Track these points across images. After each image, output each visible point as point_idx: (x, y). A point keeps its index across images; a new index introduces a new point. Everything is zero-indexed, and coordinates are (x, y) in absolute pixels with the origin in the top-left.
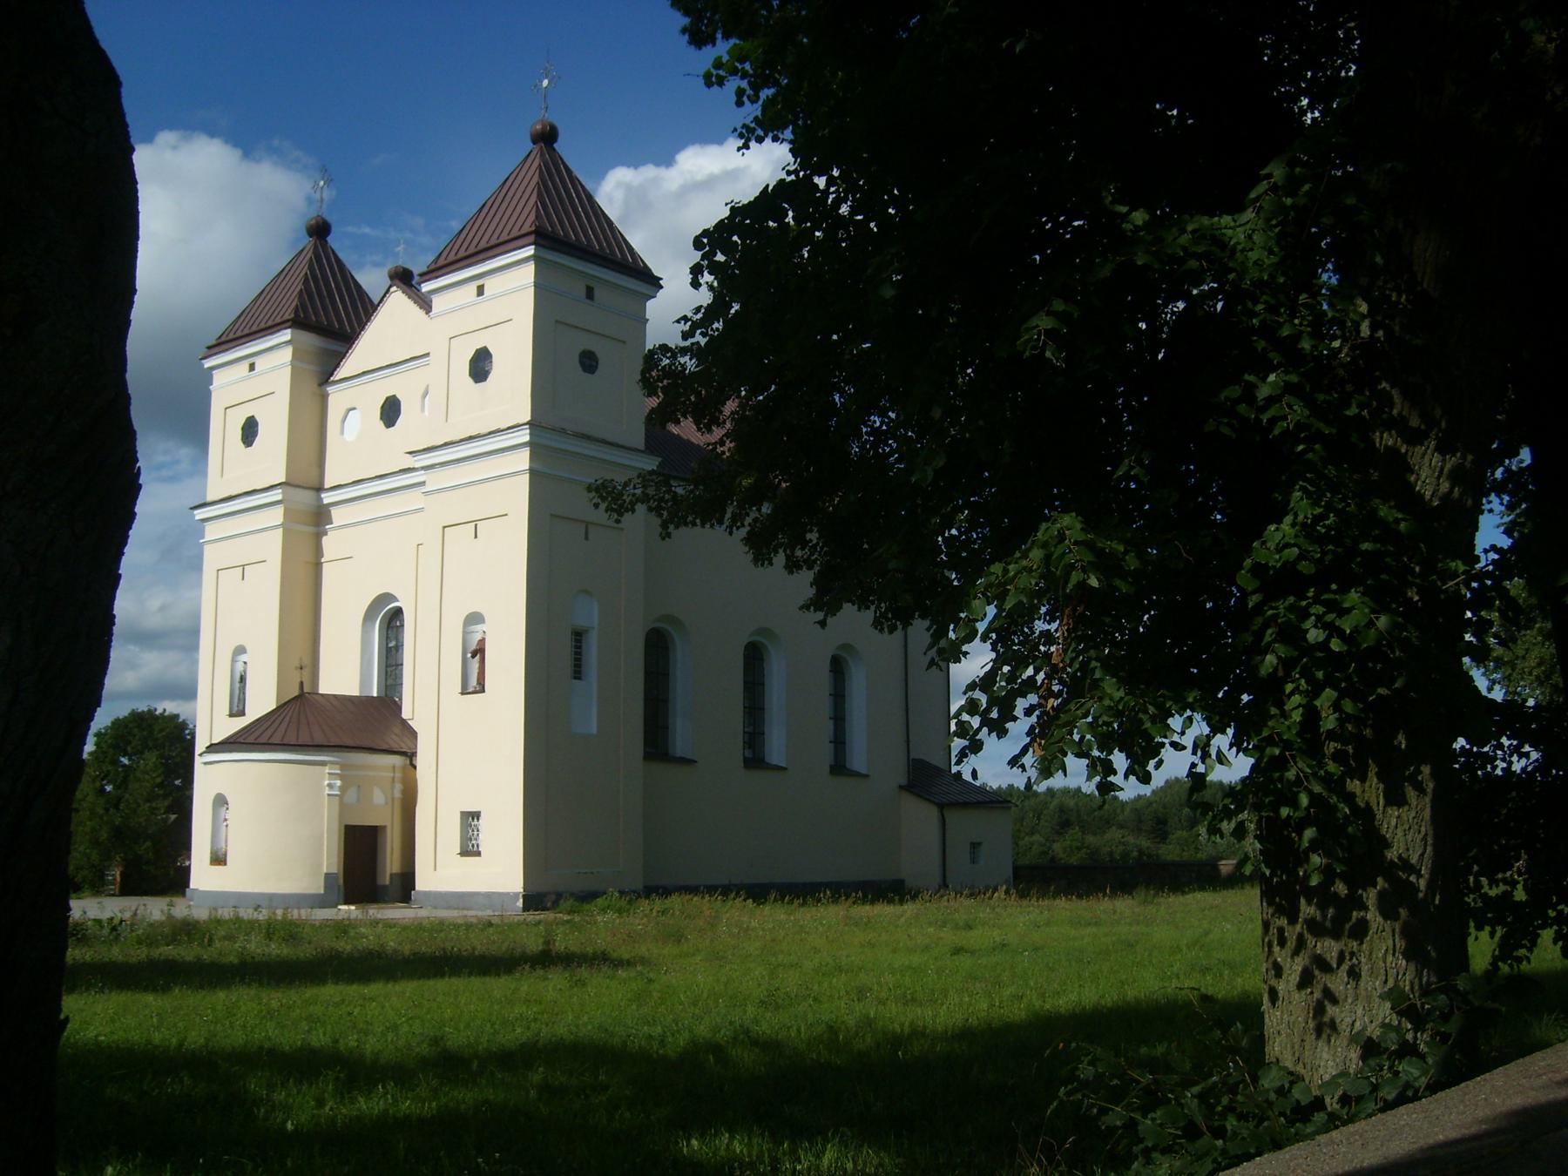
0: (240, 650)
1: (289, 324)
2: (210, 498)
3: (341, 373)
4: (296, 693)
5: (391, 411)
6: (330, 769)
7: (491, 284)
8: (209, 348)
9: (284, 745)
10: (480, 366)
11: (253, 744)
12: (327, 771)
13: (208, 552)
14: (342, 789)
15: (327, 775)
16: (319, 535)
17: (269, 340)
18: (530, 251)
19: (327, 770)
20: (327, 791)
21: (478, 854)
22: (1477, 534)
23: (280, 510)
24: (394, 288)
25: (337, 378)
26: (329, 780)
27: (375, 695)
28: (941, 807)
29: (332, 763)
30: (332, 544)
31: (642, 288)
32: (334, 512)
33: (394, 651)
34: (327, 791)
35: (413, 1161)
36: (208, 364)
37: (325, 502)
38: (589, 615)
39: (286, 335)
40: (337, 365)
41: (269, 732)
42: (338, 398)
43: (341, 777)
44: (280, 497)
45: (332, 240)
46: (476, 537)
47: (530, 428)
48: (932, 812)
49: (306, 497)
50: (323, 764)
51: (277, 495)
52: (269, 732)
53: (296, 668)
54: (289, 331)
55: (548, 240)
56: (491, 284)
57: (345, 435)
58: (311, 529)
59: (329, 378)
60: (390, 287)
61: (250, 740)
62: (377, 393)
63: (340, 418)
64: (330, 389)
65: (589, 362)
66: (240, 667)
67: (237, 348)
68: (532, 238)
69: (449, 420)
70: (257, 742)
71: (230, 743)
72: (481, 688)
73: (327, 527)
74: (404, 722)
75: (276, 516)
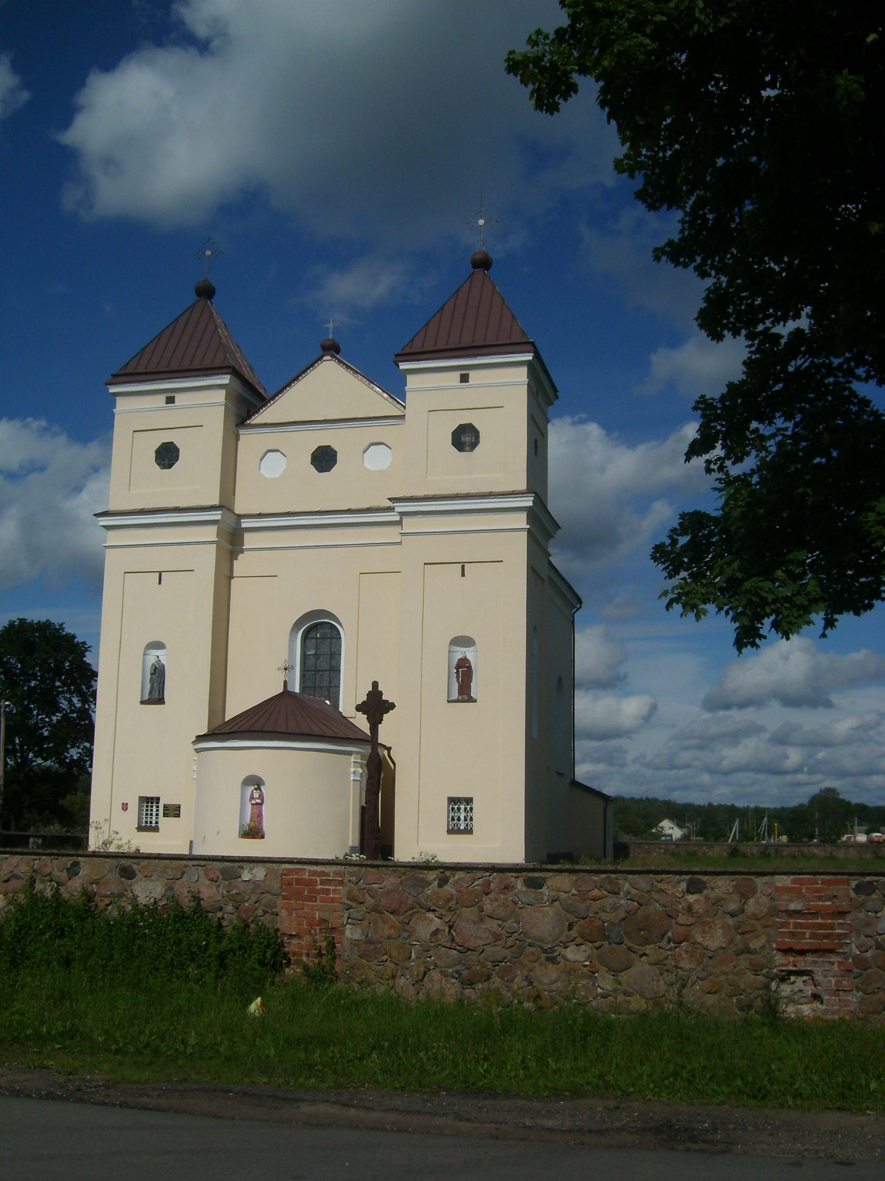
1: (231, 370)
2: (113, 507)
3: (257, 419)
4: (281, 690)
6: (354, 758)
7: (475, 376)
8: (114, 376)
9: (289, 733)
11: (229, 733)
12: (353, 760)
15: (353, 764)
17: (203, 380)
19: (352, 759)
22: (472, 683)
23: (214, 529)
24: (328, 358)
26: (354, 767)
29: (356, 753)
30: (241, 565)
32: (247, 537)
35: (479, 1105)
36: (113, 390)
37: (244, 525)
40: (257, 412)
44: (219, 517)
47: (534, 497)
50: (350, 753)
51: (216, 516)
52: (237, 727)
54: (229, 376)
56: (473, 375)
58: (229, 547)
59: (246, 421)
63: (261, 456)
66: (151, 660)
67: (157, 382)
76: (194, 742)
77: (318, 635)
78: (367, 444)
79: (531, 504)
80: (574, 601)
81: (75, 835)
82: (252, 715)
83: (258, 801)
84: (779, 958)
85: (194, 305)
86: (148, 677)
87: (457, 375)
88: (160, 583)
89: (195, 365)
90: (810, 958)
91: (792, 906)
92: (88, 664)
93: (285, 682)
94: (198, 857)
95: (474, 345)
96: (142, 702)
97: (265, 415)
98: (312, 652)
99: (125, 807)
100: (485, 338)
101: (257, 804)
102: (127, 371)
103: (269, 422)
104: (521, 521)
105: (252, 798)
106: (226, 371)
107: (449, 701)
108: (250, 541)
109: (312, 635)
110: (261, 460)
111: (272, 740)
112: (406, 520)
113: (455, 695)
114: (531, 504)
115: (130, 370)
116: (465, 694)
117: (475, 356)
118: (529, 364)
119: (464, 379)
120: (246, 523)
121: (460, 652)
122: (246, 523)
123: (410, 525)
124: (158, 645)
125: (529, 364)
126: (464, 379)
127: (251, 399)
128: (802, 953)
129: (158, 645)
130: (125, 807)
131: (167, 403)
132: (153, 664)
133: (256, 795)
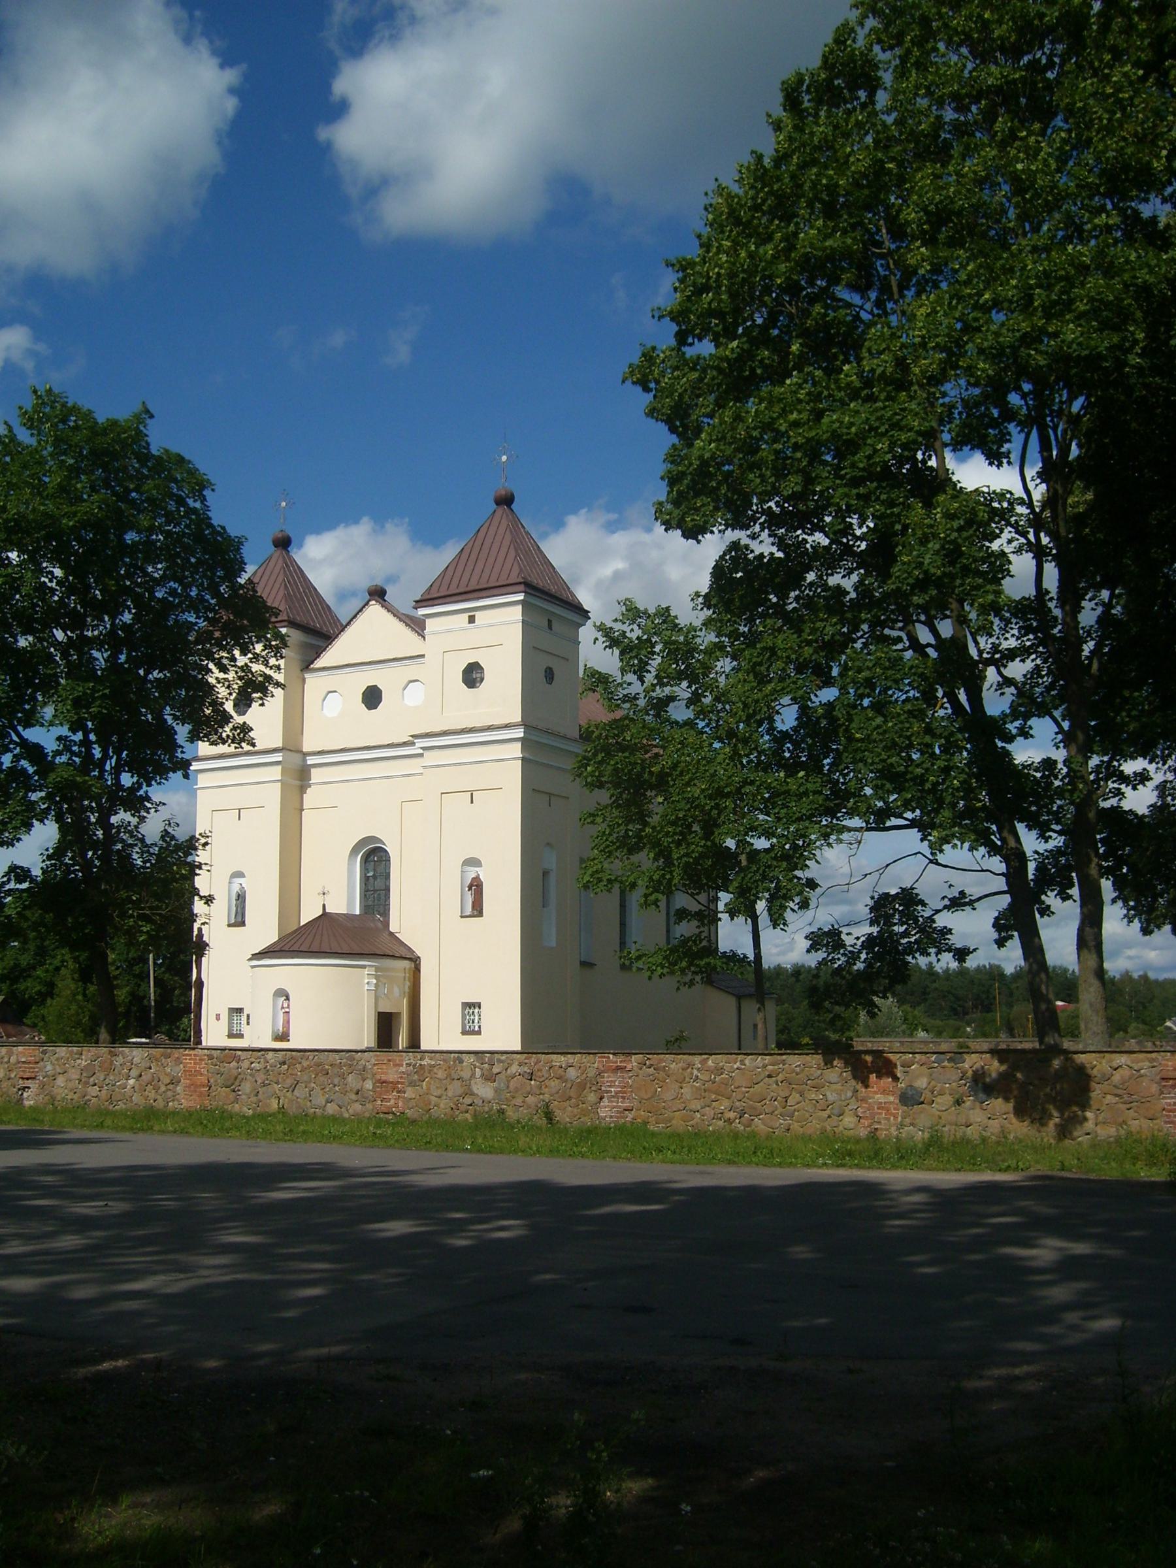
1: (286, 624)
3: (319, 664)
4: (320, 913)
5: (372, 697)
10: (472, 675)
14: (376, 985)
16: (303, 789)
18: (521, 597)
19: (366, 971)
20: (366, 987)
21: (479, 1033)
23: (279, 768)
24: (374, 602)
27: (358, 912)
28: (739, 998)
30: (309, 798)
31: (576, 618)
33: (371, 880)
34: (366, 987)
38: (551, 861)
40: (318, 656)
41: (300, 942)
43: (377, 977)
44: (280, 759)
46: (472, 802)
48: (732, 1002)
49: (296, 759)
50: (364, 967)
51: (278, 757)
52: (290, 944)
53: (319, 894)
55: (531, 588)
56: (478, 615)
57: (325, 711)
58: (298, 783)
60: (370, 601)
65: (550, 675)
66: (236, 888)
68: (522, 587)
72: (480, 913)
74: (392, 934)
75: (276, 773)
76: (250, 959)
78: (406, 682)
79: (522, 735)
84: (21, 1082)
85: (270, 558)
87: (466, 616)
90: (30, 1081)
91: (23, 1060)
93: (324, 906)
96: (229, 925)
97: (327, 659)
98: (371, 874)
99: (218, 1017)
103: (328, 665)
104: (516, 750)
105: (283, 1008)
107: (462, 917)
108: (316, 775)
110: (324, 700)
111: (293, 958)
112: (427, 754)
113: (469, 910)
114: (522, 735)
116: (478, 909)
117: (478, 599)
118: (523, 602)
119: (472, 620)
121: (472, 872)
122: (311, 761)
123: (431, 758)
124: (240, 875)
125: (523, 602)
126: (472, 620)
127: (317, 643)
128: (28, 1079)
129: (240, 875)
130: (218, 1017)
133: (285, 1005)
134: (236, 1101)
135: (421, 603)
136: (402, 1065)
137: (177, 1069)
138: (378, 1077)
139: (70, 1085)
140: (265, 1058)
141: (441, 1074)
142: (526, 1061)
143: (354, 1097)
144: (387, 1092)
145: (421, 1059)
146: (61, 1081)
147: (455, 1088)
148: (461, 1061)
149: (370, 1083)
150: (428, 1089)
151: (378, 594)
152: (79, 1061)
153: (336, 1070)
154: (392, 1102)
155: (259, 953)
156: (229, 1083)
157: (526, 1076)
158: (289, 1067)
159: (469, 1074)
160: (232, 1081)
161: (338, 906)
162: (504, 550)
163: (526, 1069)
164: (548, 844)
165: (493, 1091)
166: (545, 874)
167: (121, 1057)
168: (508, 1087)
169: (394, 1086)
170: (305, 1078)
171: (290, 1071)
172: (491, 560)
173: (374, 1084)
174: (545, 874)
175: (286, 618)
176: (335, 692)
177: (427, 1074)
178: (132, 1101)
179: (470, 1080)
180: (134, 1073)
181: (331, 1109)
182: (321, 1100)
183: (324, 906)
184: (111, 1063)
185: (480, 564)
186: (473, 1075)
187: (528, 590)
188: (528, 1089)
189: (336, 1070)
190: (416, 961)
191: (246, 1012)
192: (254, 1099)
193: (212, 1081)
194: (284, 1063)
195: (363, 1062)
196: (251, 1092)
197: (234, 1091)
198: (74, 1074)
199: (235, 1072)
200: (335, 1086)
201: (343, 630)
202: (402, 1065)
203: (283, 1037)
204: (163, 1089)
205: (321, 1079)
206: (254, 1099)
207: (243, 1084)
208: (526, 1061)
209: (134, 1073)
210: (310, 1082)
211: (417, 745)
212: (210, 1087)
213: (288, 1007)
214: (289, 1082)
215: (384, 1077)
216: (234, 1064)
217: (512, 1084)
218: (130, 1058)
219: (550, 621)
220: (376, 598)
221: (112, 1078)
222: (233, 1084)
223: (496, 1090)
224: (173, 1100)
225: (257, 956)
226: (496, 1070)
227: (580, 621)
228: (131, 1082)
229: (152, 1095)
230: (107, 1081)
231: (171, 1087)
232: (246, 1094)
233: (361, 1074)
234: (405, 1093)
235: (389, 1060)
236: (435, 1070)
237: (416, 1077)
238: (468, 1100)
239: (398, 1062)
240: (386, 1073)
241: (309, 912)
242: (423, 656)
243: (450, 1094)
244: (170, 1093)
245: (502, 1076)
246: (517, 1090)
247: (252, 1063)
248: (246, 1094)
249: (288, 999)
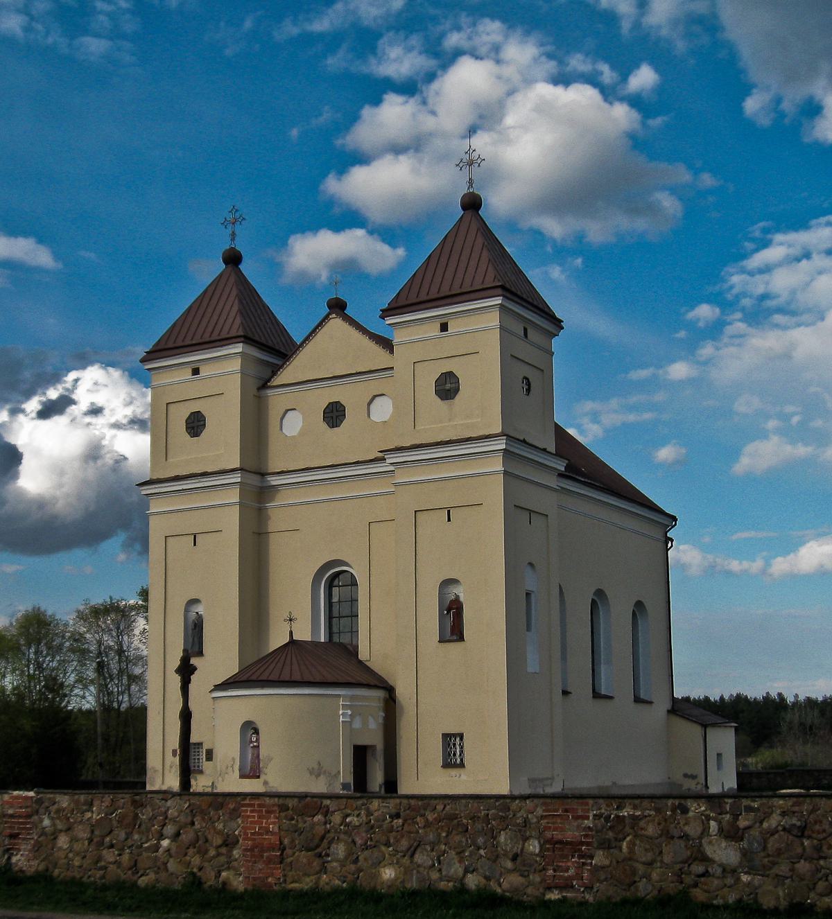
0: (194, 602)
5: (334, 415)
10: (447, 387)
13: (153, 522)
18: (498, 301)
21: (462, 765)
24: (334, 315)
25: (275, 384)
27: (323, 640)
39: (238, 348)
42: (277, 400)
44: (239, 480)
45: (243, 267)
46: (449, 520)
49: (254, 480)
51: (236, 478)
54: (241, 345)
61: (244, 678)
62: (324, 397)
64: (270, 392)
66: (192, 616)
68: (500, 291)
69: (416, 428)
70: (260, 679)
71: (228, 684)
73: (267, 505)
75: (234, 496)
77: (340, 584)
79: (504, 447)
80: (665, 521)
81: (125, 780)
82: (271, 660)
83: (255, 744)
86: (190, 632)
88: (195, 545)
89: (423, 297)
92: (821, 545)
93: (291, 633)
94: (292, 794)
95: (485, 287)
100: (483, 281)
101: (254, 747)
102: (400, 304)
106: (239, 340)
109: (336, 582)
115: (401, 302)
119: (444, 327)
120: (274, 480)
122: (274, 480)
124: (194, 602)
126: (444, 327)
131: (441, 332)
132: (193, 620)
133: (254, 739)
134: (323, 869)
135: (387, 312)
136: (587, 818)
137: (233, 824)
138: (548, 834)
139: (77, 846)
140: (368, 809)
141: (651, 830)
142: (796, 809)
143: (509, 865)
144: (566, 857)
145: (618, 808)
146: (63, 841)
147: (672, 852)
148: (685, 810)
149: (536, 843)
150: (631, 850)
151: (338, 307)
152: (88, 815)
153: (479, 826)
154: (571, 872)
155: (223, 684)
156: (312, 845)
157: (795, 832)
158: (405, 820)
159: (699, 830)
160: (316, 841)
161: (303, 633)
162: (475, 255)
163: (794, 821)
164: (531, 564)
165: (738, 854)
166: (528, 594)
167: (149, 809)
168: (765, 848)
169: (574, 847)
170: (431, 837)
171: (406, 826)
172: (462, 265)
173: (541, 846)
174: (528, 594)
175: (242, 334)
176: (295, 409)
177: (628, 829)
178: (167, 870)
179: (700, 838)
180: (170, 829)
181: (472, 881)
182: (457, 869)
183: (291, 633)
184: (136, 816)
185: (451, 269)
186: (706, 830)
187: (505, 293)
188: (799, 850)
189: (479, 826)
190: (390, 690)
191: (205, 747)
192: (353, 867)
193: (286, 841)
194: (398, 816)
195: (523, 813)
196: (346, 858)
197: (320, 856)
198: (82, 833)
199: (320, 830)
200: (479, 848)
201: (298, 349)
202: (587, 818)
203: (252, 771)
204: (212, 852)
205: (457, 838)
206: (353, 867)
207: (334, 846)
208: (796, 809)
209: (170, 829)
210: (439, 842)
211: (388, 461)
212: (284, 849)
213: (257, 740)
214: (404, 844)
215: (557, 835)
216: (319, 818)
217: (773, 844)
218: (163, 809)
219: (525, 330)
220: (337, 310)
221: (136, 837)
222: (318, 846)
223: (745, 854)
224: (228, 868)
225: (218, 687)
226: (742, 823)
227: (554, 331)
228: (165, 843)
229: (196, 860)
230: (130, 842)
231: (224, 850)
232: (337, 861)
233: (520, 831)
234: (592, 857)
235: (566, 811)
236: (642, 824)
237: (611, 834)
238: (698, 868)
239: (580, 813)
240: (562, 830)
241: (277, 639)
242: (392, 368)
243: (667, 859)
244: (223, 859)
245: (755, 832)
246: (779, 852)
247: (348, 816)
248: (337, 861)
249: (256, 731)
